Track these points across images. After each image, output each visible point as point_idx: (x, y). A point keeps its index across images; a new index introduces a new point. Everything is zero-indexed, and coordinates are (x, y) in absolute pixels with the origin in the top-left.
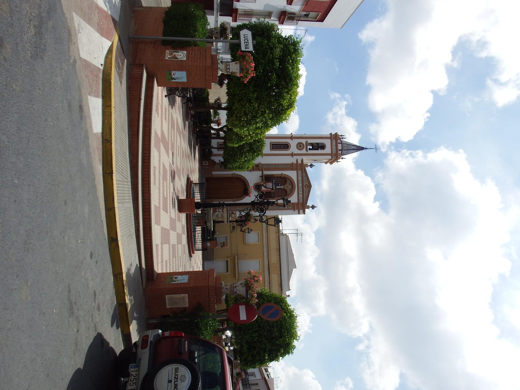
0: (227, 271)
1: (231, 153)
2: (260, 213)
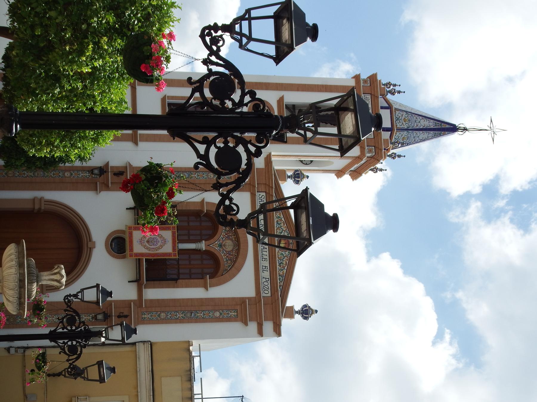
1: (38, 32)
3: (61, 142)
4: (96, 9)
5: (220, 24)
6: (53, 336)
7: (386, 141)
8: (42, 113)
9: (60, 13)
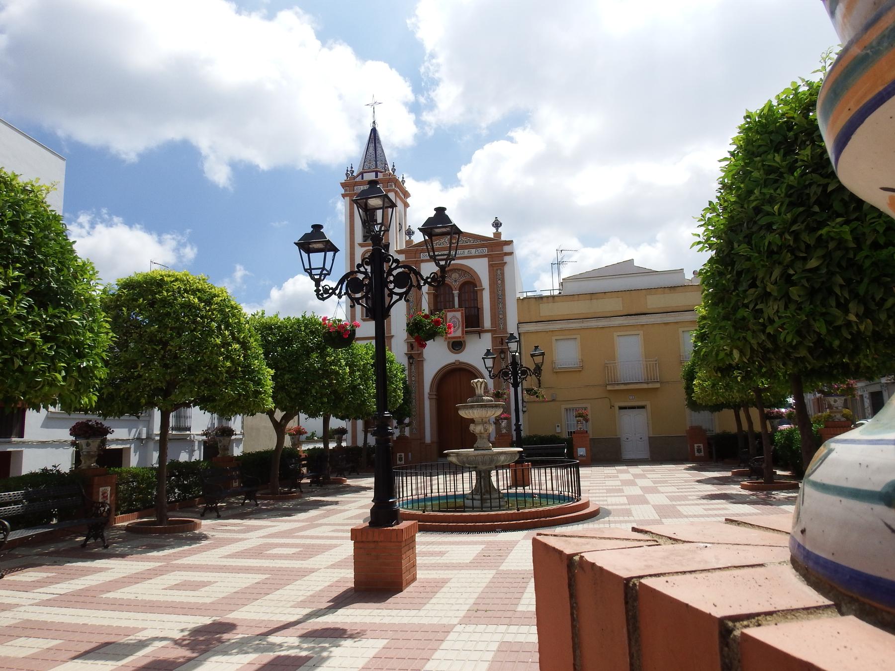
0: (643, 407)
1: (326, 400)
2: (412, 286)
3: (393, 384)
4: (309, 365)
5: (316, 288)
6: (516, 385)
7: (384, 175)
8: (377, 396)
9: (313, 387)
